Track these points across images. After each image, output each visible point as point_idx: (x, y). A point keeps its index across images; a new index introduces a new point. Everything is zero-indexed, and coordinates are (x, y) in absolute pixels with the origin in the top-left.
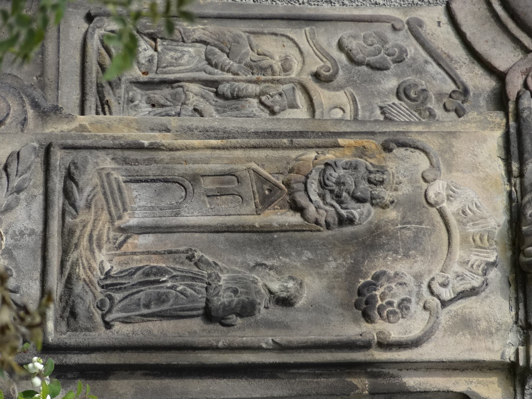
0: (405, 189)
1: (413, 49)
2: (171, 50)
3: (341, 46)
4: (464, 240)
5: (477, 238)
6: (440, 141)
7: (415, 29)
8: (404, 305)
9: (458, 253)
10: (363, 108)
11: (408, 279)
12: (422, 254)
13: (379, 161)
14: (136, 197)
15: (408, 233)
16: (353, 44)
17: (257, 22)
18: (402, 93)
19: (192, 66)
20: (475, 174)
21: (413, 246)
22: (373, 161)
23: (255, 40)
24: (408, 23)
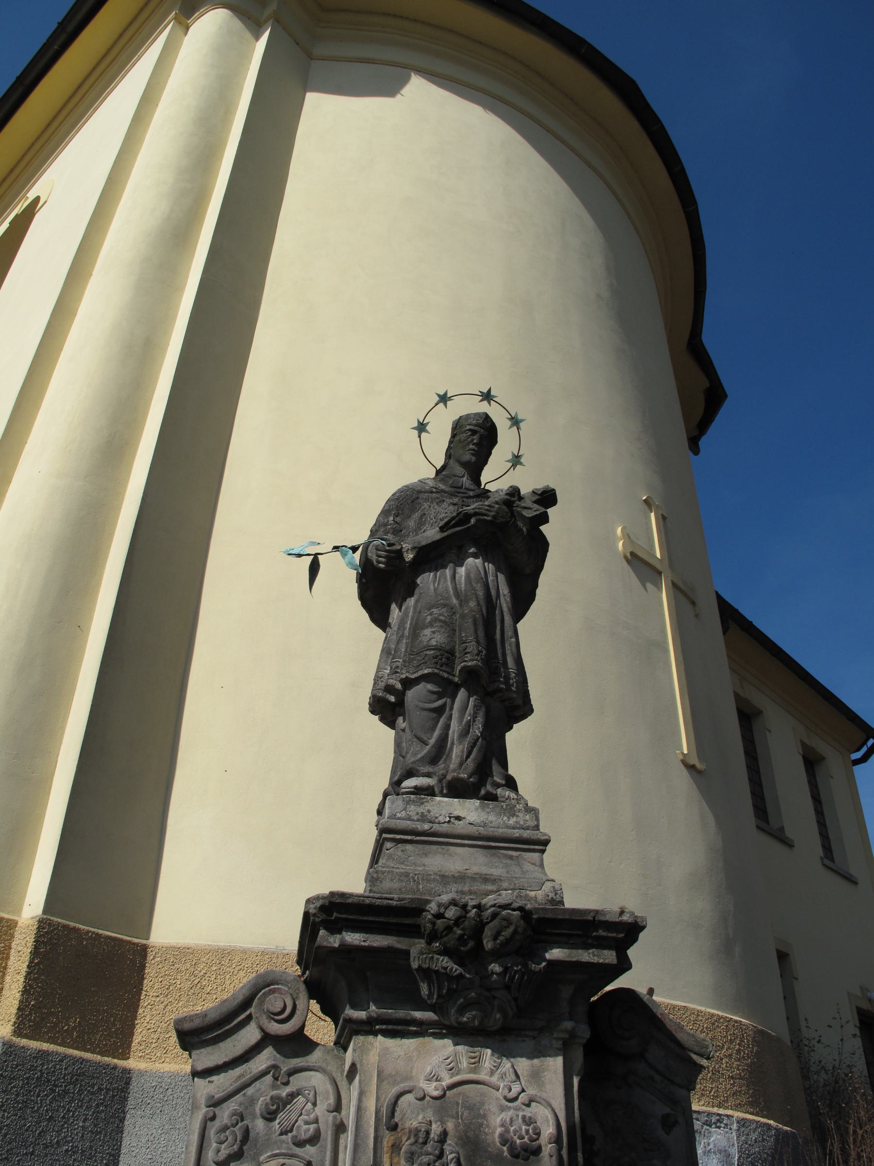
0: (430, 1115)
1: (232, 1106)
4: (474, 1071)
5: (473, 1061)
6: (385, 1083)
7: (216, 1103)
8: (528, 1121)
9: (483, 1076)
10: (279, 1149)
11: (507, 1116)
12: (483, 1104)
13: (405, 1134)
15: (466, 1114)
18: (270, 1116)
20: (415, 1059)
21: (477, 1114)
22: (404, 1139)
24: (209, 1106)
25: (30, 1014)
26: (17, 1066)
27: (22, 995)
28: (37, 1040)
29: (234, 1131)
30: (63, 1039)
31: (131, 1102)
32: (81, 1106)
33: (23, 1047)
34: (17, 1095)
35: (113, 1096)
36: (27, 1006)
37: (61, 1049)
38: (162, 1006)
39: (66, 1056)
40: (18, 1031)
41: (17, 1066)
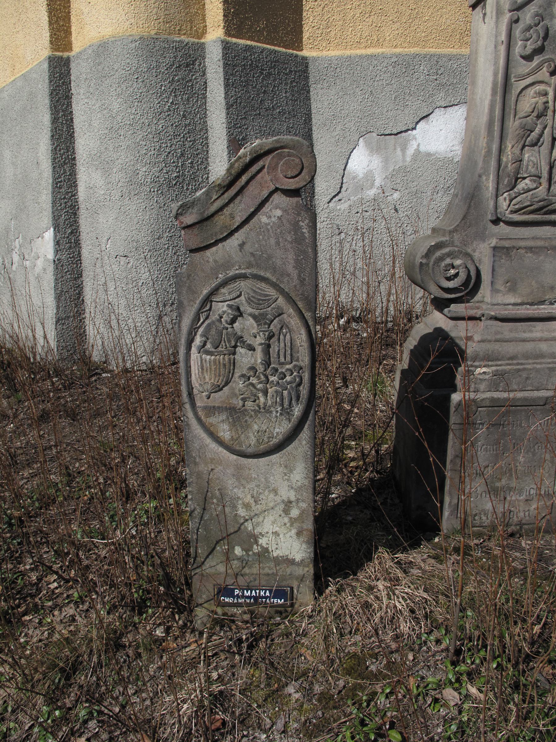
2: (527, 168)
3: (528, 58)
14: (178, 505)
16: (530, 47)
17: (507, 110)
19: (537, 155)
23: (521, 114)
24: (514, 11)
25: (233, 19)
26: (235, 56)
27: (224, 5)
28: (242, 39)
29: (537, 30)
30: (258, 37)
31: (312, 80)
32: (282, 83)
33: (235, 44)
34: (241, 77)
35: (300, 76)
36: (229, 13)
37: (259, 45)
38: (320, 8)
39: (264, 49)
40: (228, 33)
41: (235, 56)
